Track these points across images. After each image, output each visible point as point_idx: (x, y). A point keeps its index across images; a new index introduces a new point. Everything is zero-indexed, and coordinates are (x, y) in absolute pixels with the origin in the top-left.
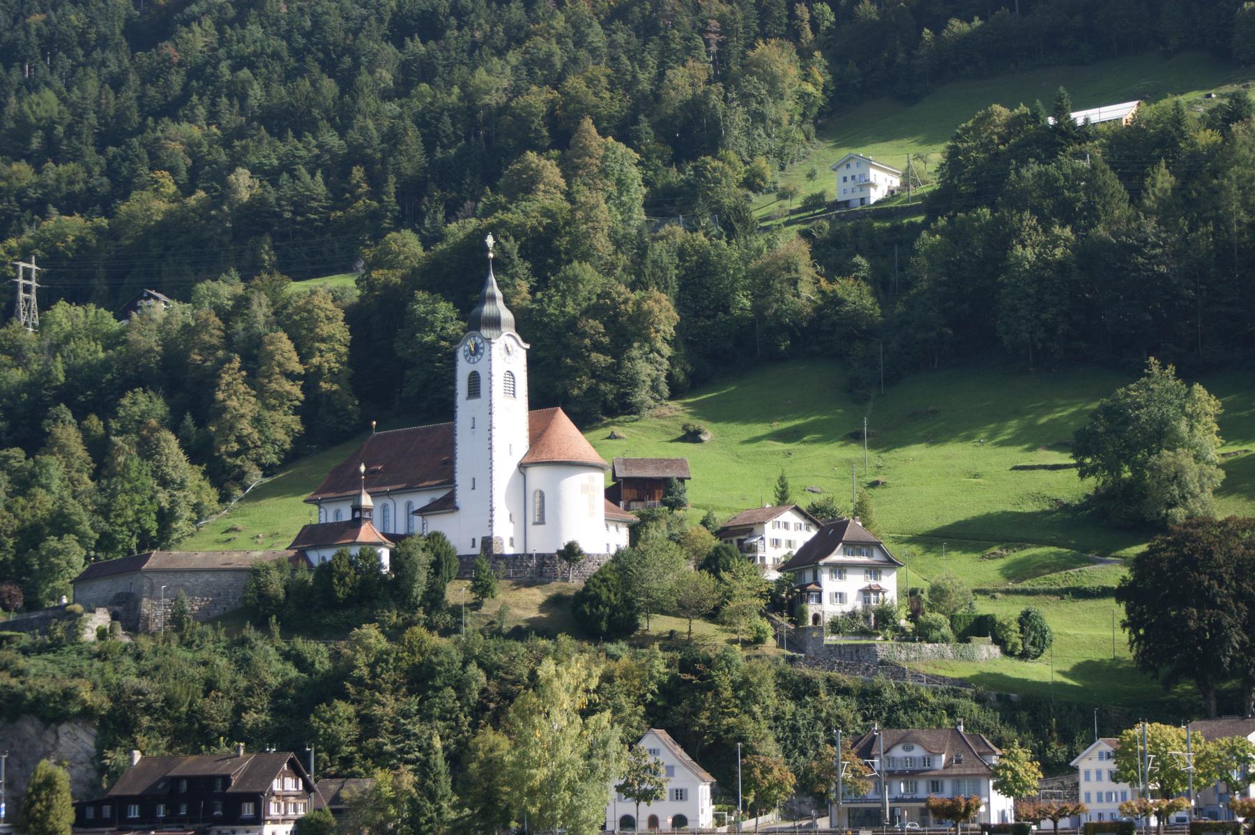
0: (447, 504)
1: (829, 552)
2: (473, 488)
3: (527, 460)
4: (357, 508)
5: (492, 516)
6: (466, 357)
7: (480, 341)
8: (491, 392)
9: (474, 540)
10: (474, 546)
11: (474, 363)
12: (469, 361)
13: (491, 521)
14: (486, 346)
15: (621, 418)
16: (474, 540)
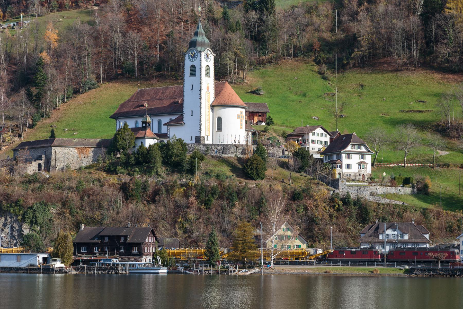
0: (179, 122)
1: (346, 146)
2: (192, 115)
3: (214, 104)
5: (200, 127)
6: (189, 58)
7: (196, 52)
8: (201, 74)
9: (192, 137)
10: (192, 140)
11: (193, 61)
12: (190, 61)
13: (200, 129)
14: (199, 54)
16: (192, 137)
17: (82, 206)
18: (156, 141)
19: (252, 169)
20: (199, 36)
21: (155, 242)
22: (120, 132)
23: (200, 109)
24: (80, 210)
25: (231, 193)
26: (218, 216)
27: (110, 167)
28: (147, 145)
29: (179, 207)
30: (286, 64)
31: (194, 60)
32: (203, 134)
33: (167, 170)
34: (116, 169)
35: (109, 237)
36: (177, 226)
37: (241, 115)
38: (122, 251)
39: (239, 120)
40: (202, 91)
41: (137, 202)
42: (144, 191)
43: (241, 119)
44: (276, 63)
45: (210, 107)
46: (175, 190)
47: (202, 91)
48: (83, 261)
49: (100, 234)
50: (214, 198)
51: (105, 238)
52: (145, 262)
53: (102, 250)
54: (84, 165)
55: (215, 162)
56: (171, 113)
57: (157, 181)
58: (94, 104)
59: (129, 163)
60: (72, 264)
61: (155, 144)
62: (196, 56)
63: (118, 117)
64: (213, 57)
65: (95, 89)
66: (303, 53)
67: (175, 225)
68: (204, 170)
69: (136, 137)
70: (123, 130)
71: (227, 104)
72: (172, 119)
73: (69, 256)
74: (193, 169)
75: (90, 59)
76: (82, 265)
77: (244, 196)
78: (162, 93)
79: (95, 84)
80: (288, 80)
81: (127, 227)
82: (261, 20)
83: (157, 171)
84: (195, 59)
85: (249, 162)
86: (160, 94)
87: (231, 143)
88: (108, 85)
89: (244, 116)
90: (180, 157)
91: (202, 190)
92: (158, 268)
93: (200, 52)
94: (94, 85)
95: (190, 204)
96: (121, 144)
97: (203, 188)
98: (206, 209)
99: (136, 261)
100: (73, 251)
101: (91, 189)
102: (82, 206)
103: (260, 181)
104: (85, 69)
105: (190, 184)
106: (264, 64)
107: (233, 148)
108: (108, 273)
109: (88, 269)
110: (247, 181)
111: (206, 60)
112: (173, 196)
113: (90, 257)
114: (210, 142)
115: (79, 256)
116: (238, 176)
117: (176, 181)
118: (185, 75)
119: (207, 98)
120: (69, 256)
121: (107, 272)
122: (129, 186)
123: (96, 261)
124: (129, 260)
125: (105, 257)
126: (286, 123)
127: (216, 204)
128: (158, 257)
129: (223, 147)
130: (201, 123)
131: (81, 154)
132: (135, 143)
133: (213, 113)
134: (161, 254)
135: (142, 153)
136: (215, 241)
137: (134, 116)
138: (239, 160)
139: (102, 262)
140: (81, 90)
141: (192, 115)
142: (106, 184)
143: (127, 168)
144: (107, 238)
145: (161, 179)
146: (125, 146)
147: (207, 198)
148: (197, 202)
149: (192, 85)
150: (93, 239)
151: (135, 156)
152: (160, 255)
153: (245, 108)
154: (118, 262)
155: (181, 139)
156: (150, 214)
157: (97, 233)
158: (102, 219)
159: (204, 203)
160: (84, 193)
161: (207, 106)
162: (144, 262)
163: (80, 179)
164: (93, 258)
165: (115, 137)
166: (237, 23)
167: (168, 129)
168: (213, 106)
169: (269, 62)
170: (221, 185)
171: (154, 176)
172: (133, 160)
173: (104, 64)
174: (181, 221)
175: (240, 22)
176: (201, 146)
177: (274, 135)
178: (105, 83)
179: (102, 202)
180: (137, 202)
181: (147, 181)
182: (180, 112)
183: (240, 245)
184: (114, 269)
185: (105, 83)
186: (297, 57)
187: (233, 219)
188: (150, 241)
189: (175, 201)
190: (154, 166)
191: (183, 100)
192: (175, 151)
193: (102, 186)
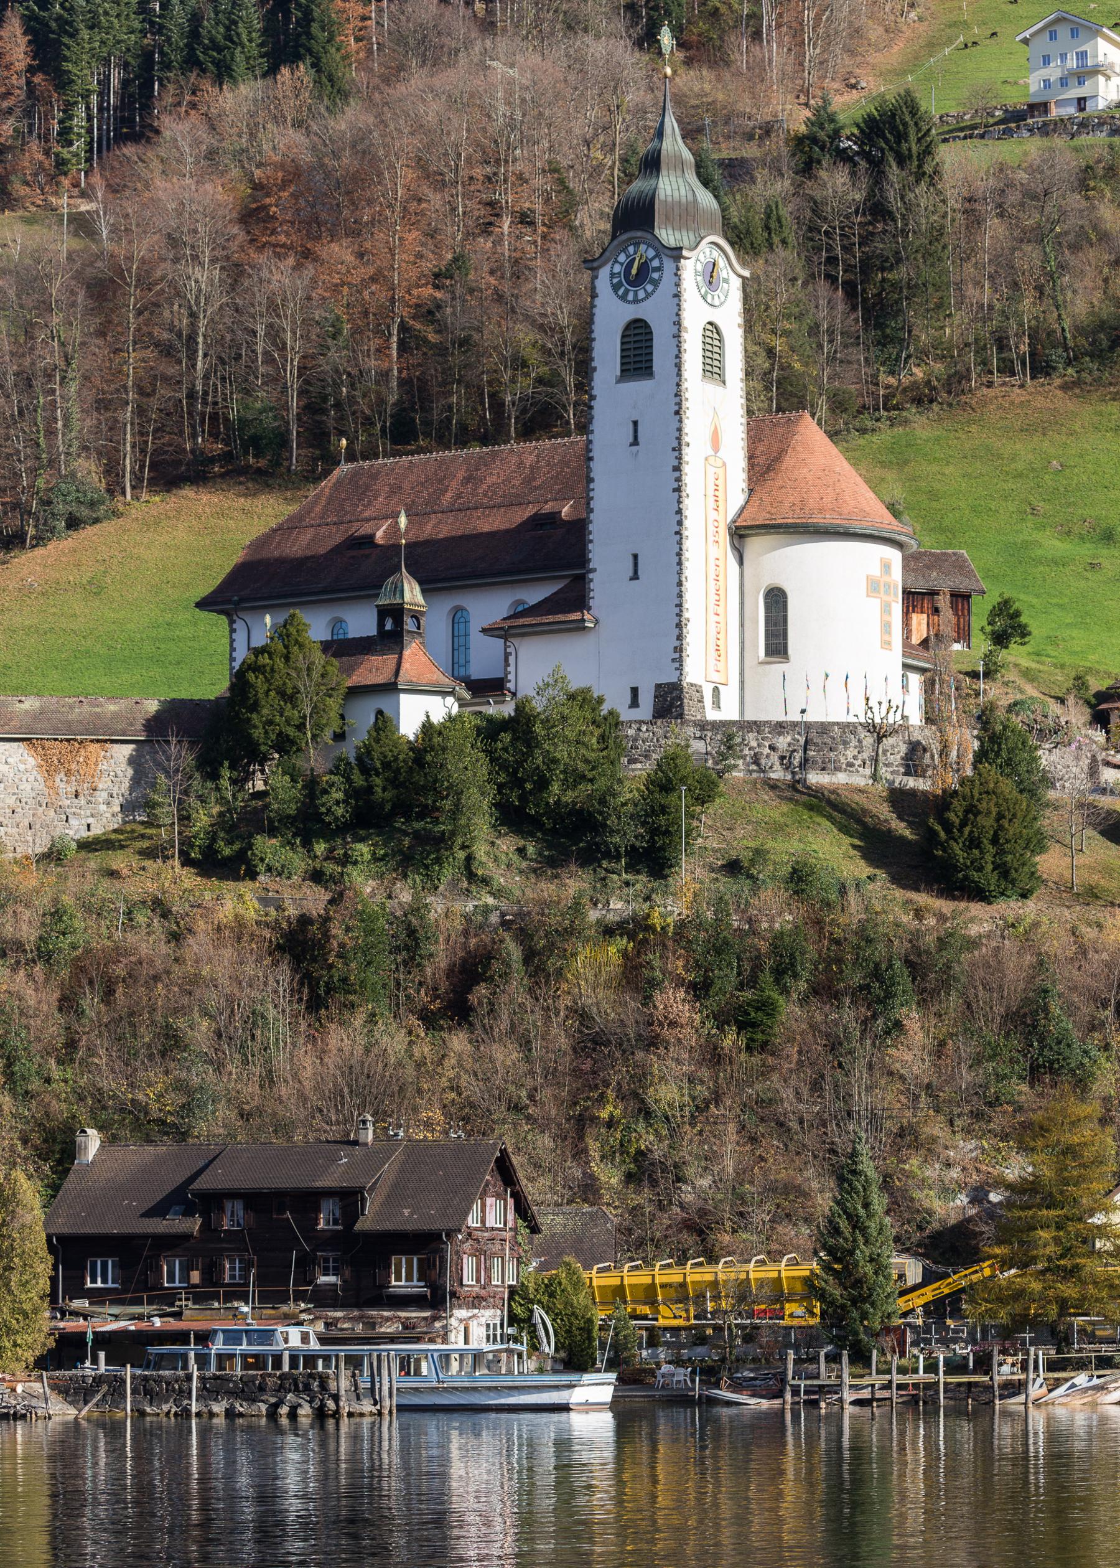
2: (635, 577)
3: (747, 520)
4: (396, 612)
5: (680, 637)
6: (616, 288)
7: (651, 253)
9: (635, 691)
10: (634, 703)
11: (636, 301)
12: (623, 298)
14: (669, 265)
15: (819, 1512)
16: (635, 691)
17: (71, 1044)
18: (451, 706)
19: (974, 843)
20: (664, 172)
21: (515, 1229)
22: (265, 660)
23: (680, 543)
24: (60, 1062)
25: (877, 965)
26: (816, 1086)
27: (214, 839)
28: (409, 726)
29: (599, 1041)
30: (1000, 407)
31: (641, 294)
32: (695, 671)
33: (521, 851)
34: (250, 846)
35: (254, 1200)
36: (593, 1146)
37: (886, 578)
38: (332, 1279)
39: (875, 604)
40: (689, 454)
41: (372, 1019)
42: (405, 963)
43: (885, 598)
44: (950, 405)
45: (724, 538)
46: (574, 955)
47: (685, 450)
48: (103, 1340)
49: (195, 1186)
50: (785, 991)
51: (228, 1205)
52: (466, 1342)
53: (212, 1275)
54: (76, 830)
55: (775, 809)
56: (520, 572)
57: (470, 908)
58: (95, 589)
59: (318, 817)
60: (42, 1363)
61: (451, 719)
62: (655, 275)
63: (241, 600)
64: (736, 283)
65: (98, 526)
66: (1076, 358)
67: (581, 1137)
68: (715, 851)
69: (349, 683)
70: (280, 646)
71: (817, 519)
72: (523, 602)
73: (26, 1316)
74: (662, 849)
75: (73, 388)
76: (103, 1368)
77: (946, 983)
78: (467, 480)
79: (101, 502)
80: (1020, 475)
81: (356, 1143)
82: (877, 209)
83: (469, 858)
84: (650, 288)
85: (958, 805)
86: (454, 484)
87: (843, 718)
88: (156, 503)
89: (896, 587)
90: (591, 781)
91: (718, 952)
92: (565, 1378)
93: (676, 254)
94: (92, 504)
95: (661, 1024)
96: (270, 722)
97: (726, 942)
98: (749, 1048)
99: (418, 1340)
100: (44, 1284)
101: (119, 952)
102: (71, 1044)
103: (1009, 907)
104: (51, 433)
105: (656, 920)
106: (896, 408)
107: (854, 743)
108: (272, 1414)
109: (146, 1390)
110: (946, 906)
111: (704, 298)
112: (565, 986)
113: (140, 1317)
114: (729, 712)
115: (76, 1314)
116: (899, 880)
117: (577, 907)
118: (596, 375)
119: (710, 492)
120: (26, 1316)
121: (264, 1408)
122: (327, 935)
123: (181, 1337)
124: (370, 1333)
125: (236, 1314)
126: (1053, 654)
127: (804, 1026)
128: (538, 1312)
129: (802, 740)
130: (686, 615)
131: (59, 778)
132: (342, 717)
133: (741, 563)
134: (552, 1295)
135: (386, 765)
136: (870, 1216)
137: (324, 592)
138: (900, 799)
139: (218, 1346)
140: (31, 531)
141: (635, 577)
142: (201, 925)
143: (307, 844)
144: (239, 1206)
145: (490, 901)
146: (291, 732)
147: (748, 995)
148: (697, 1018)
149: (635, 423)
150: (159, 1210)
151: (349, 780)
152: (545, 1299)
153: (899, 545)
154: (314, 1345)
155: (589, 690)
156: (444, 1083)
157: (179, 1179)
158: (186, 1109)
159: (737, 1022)
160: (83, 969)
161: (711, 529)
162: (457, 1341)
163: (56, 901)
164: (157, 1322)
165: (240, 682)
166: (769, 217)
167: (507, 655)
168: (739, 534)
169: (918, 401)
170: (819, 923)
171: (453, 884)
172: (338, 803)
173: (140, 411)
174: (611, 1116)
175: (785, 211)
176: (691, 731)
177: (1031, 691)
178: (145, 496)
179: (181, 1024)
180: (372, 1019)
181: (417, 909)
182: (570, 567)
183: (1044, 1234)
184: (307, 1388)
185: (145, 496)
186: (1048, 374)
187: (889, 1097)
188: (491, 1222)
189: (582, 1015)
190: (453, 833)
191: (586, 501)
192: (562, 753)
193: (175, 937)
